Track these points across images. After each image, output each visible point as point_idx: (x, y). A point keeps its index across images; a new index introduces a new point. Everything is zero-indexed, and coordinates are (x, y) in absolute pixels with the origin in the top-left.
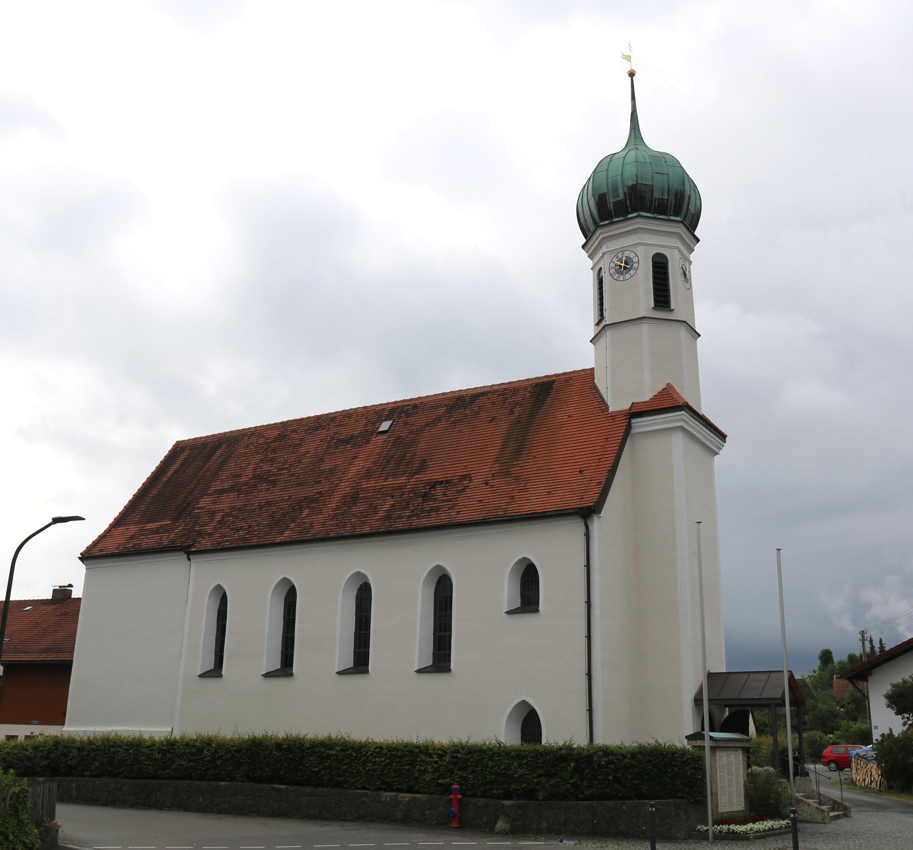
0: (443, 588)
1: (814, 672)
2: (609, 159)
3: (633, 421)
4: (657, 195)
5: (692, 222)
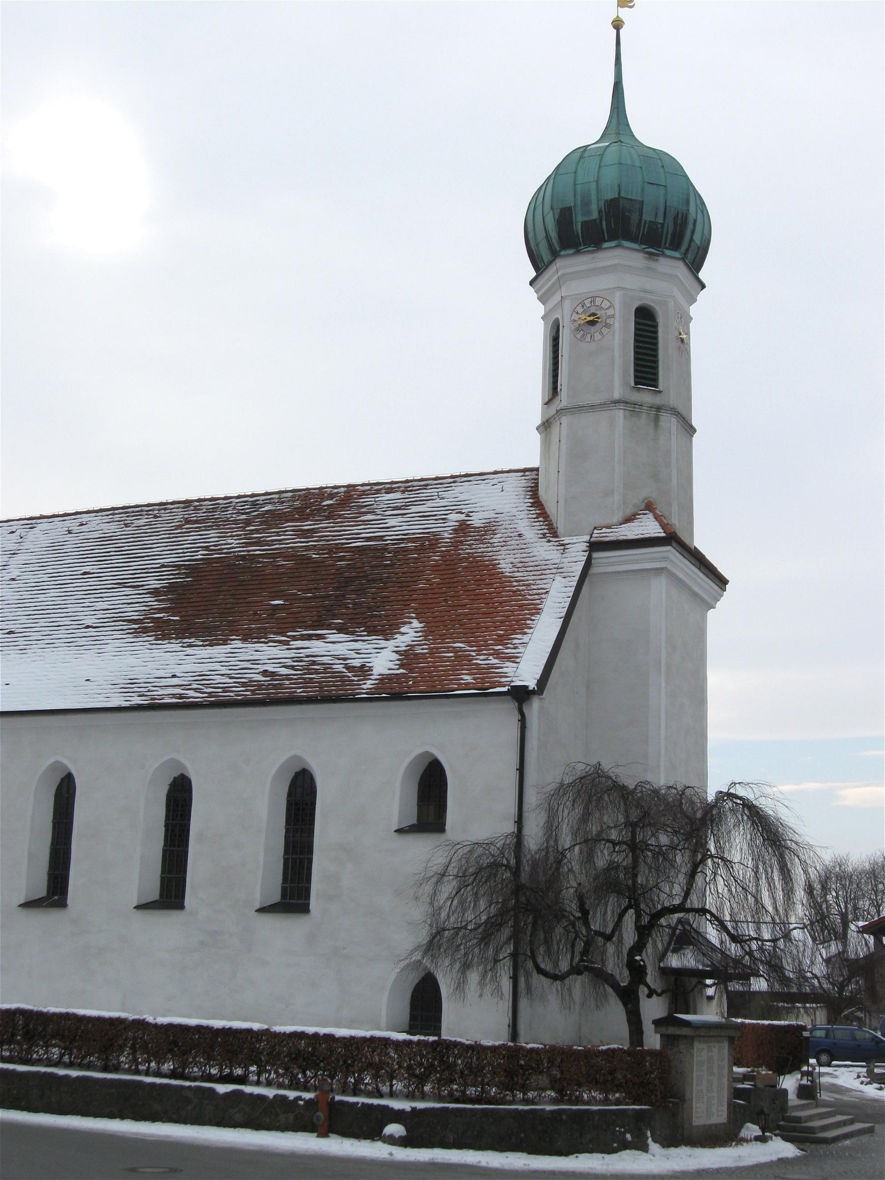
0: (301, 799)
1: (823, 926)
2: (578, 155)
3: (595, 555)
4: (647, 217)
5: (695, 260)
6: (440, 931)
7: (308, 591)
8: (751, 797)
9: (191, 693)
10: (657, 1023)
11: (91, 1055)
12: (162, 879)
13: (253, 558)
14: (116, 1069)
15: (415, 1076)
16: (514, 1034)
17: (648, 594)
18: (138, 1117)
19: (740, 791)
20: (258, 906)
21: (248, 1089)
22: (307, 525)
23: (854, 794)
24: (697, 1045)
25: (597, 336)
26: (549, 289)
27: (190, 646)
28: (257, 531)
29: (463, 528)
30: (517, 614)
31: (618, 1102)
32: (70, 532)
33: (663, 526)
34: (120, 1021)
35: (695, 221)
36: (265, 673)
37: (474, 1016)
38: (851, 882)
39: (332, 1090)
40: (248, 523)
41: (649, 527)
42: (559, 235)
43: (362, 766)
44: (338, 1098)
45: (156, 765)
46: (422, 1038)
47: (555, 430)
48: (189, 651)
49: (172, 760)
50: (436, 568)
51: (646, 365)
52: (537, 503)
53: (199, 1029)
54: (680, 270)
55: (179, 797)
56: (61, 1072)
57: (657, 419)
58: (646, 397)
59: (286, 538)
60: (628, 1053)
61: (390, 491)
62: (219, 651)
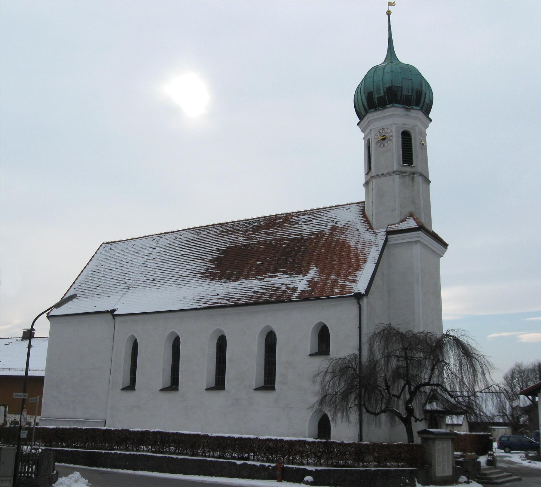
0: (270, 342)
2: (374, 69)
3: (389, 237)
4: (405, 93)
5: (427, 109)
6: (325, 397)
7: (271, 257)
8: (456, 336)
9: (225, 301)
10: (419, 433)
11: (187, 450)
12: (216, 378)
13: (248, 245)
14: (197, 455)
15: (318, 456)
16: (361, 439)
17: (414, 253)
18: (205, 475)
19: (451, 333)
20: (254, 388)
21: (249, 462)
22: (271, 231)
23: (526, 337)
24: (437, 442)
25: (386, 145)
26: (365, 126)
27: (224, 282)
28: (250, 234)
29: (334, 228)
30: (355, 262)
31: (403, 466)
32: (176, 238)
33: (417, 223)
34: (198, 435)
35: (426, 93)
36: (254, 292)
37: (343, 432)
38: (524, 374)
39: (284, 463)
40: (247, 231)
41: (411, 224)
42: (368, 103)
43: (295, 328)
44: (285, 466)
45: (212, 332)
46: (320, 440)
47: (370, 185)
48: (224, 284)
49: (218, 329)
50: (323, 246)
51: (407, 156)
52: (364, 216)
53: (229, 437)
54: (420, 115)
55: (221, 344)
56: (175, 456)
57: (413, 178)
58: (408, 169)
59: (262, 236)
60: (407, 445)
61: (304, 215)
62: (236, 284)
